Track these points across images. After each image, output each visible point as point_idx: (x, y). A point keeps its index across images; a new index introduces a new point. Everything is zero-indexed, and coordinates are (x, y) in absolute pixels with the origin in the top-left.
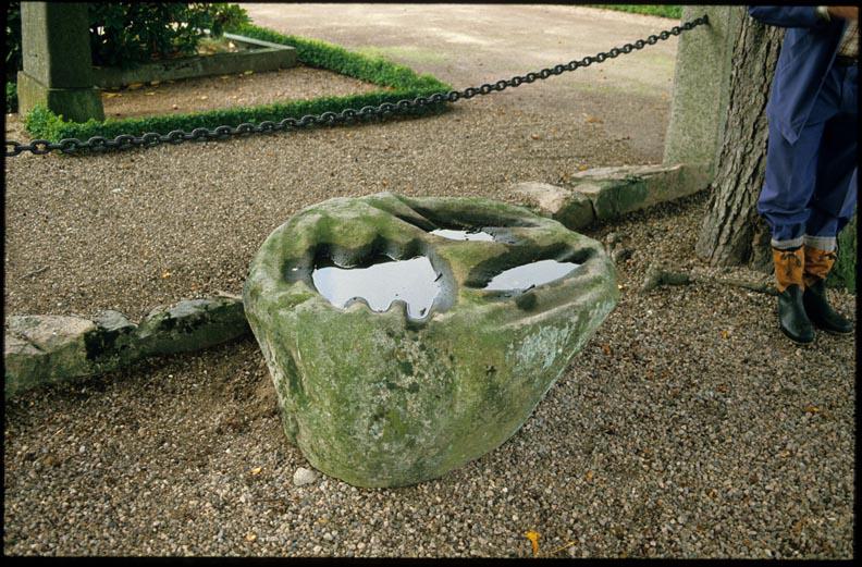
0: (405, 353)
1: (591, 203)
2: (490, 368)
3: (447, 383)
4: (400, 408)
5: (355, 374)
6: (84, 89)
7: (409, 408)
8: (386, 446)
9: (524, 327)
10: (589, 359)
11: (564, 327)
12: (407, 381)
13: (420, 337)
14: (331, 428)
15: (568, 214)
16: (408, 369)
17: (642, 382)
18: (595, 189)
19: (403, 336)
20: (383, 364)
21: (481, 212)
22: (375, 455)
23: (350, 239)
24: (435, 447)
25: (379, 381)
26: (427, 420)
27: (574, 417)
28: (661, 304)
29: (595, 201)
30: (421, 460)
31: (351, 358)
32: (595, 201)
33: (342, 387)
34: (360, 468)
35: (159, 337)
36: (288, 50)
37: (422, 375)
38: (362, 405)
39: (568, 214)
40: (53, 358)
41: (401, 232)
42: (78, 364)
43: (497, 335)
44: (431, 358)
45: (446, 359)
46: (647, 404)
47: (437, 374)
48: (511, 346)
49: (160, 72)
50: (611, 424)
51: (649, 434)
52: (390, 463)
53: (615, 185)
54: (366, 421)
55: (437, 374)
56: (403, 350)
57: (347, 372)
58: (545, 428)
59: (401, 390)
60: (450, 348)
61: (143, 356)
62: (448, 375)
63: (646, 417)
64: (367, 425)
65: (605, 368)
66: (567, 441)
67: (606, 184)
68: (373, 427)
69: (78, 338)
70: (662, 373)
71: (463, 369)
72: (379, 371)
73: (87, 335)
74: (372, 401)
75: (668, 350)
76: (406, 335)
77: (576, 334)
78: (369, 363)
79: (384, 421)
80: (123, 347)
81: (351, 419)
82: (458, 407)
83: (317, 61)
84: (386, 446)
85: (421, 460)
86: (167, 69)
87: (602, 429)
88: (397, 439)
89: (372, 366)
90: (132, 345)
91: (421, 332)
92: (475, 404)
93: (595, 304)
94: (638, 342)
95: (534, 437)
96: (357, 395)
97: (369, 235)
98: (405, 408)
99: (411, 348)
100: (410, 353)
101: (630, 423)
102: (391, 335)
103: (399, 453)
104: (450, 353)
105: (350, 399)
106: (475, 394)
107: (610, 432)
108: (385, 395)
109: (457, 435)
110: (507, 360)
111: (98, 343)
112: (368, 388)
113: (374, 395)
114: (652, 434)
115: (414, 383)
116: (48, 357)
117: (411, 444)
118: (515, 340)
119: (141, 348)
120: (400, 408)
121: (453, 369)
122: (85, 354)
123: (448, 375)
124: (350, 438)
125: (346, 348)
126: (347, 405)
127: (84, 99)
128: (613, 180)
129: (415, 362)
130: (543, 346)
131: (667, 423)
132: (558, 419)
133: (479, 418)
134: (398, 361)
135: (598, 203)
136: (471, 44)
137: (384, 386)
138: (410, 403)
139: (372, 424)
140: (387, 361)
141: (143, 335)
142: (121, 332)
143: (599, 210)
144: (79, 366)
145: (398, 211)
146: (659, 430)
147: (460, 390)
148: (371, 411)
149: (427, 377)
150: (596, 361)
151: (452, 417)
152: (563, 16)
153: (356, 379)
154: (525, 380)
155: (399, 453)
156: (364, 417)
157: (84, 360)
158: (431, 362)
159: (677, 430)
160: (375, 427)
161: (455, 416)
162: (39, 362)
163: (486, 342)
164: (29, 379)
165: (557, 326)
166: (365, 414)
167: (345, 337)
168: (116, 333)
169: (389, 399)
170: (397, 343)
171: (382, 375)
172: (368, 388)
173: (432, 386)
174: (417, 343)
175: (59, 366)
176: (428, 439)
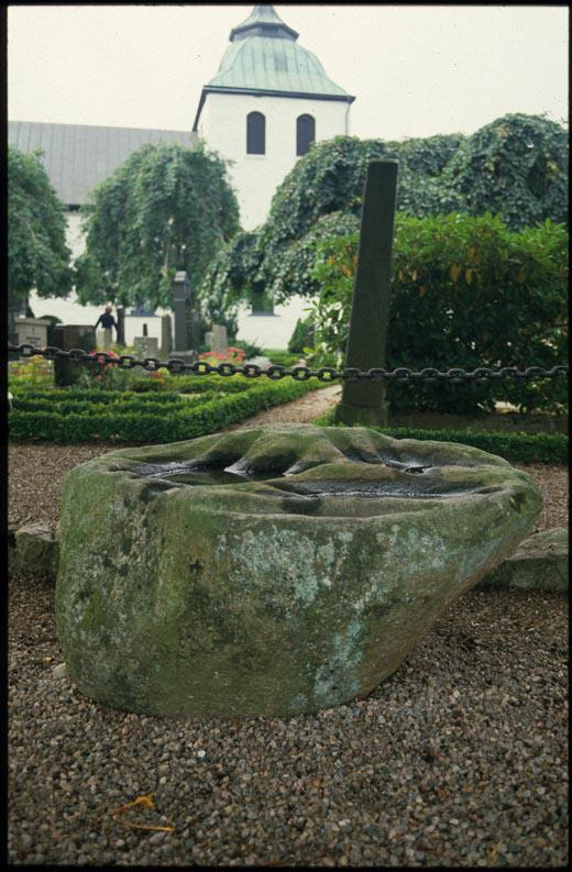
11: (326, 543)
12: (122, 559)
25: (99, 554)
38: (75, 577)
45: (159, 541)
48: (224, 539)
85: (121, 672)
89: (98, 535)
92: (177, 609)
98: (109, 592)
113: (88, 568)
115: (126, 565)
117: (106, 640)
120: (104, 591)
130: (283, 558)
137: (101, 561)
138: (115, 587)
139: (76, 602)
140: (114, 533)
143: (514, 402)
147: (161, 583)
149: (139, 560)
151: (150, 620)
153: (81, 546)
156: (73, 592)
158: (147, 542)
160: (78, 607)
161: (155, 620)
164: (34, 562)
165: (310, 535)
166: (73, 588)
171: (104, 548)
176: (124, 644)
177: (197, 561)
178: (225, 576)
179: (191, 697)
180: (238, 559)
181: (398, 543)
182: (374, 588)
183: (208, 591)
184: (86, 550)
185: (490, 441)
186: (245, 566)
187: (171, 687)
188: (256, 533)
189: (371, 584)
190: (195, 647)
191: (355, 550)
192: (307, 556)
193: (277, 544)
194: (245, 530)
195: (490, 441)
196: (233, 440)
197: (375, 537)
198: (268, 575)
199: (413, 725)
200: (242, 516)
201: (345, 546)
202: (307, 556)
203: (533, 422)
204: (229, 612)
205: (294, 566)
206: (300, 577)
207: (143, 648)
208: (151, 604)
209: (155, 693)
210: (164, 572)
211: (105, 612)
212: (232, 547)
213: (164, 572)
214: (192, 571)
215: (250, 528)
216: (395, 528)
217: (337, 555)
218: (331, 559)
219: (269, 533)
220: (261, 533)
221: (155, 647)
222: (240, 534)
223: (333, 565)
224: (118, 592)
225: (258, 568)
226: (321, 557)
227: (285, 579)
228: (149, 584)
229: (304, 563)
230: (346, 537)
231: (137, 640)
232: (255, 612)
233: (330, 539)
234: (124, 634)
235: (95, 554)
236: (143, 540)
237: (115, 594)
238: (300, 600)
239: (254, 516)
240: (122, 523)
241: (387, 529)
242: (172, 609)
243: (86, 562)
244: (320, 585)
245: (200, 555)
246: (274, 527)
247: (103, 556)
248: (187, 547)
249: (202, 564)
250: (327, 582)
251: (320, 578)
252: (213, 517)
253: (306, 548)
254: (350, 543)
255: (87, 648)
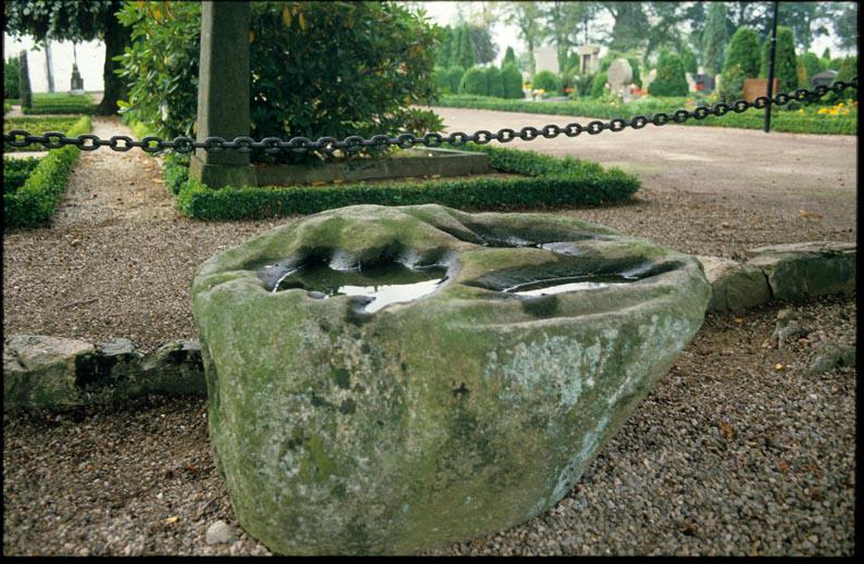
0: (343, 355)
1: (767, 277)
2: (458, 386)
3: (396, 403)
4: (326, 435)
5: (270, 380)
6: (238, 166)
7: (338, 435)
8: (302, 490)
9: (517, 331)
10: (694, 439)
11: (592, 343)
12: (340, 395)
13: (364, 334)
14: (236, 455)
15: (729, 287)
16: (343, 379)
17: (765, 473)
18: (771, 261)
19: (342, 332)
20: (309, 369)
21: (549, 228)
22: (288, 502)
23: (356, 241)
24: (377, 501)
25: (301, 392)
26: (362, 455)
27: (637, 506)
28: (834, 389)
29: (771, 275)
30: (358, 522)
31: (267, 357)
32: (771, 275)
33: (250, 395)
34: (271, 520)
35: (166, 371)
36: (480, 156)
37: (360, 389)
38: (273, 423)
39: (729, 287)
40: (33, 379)
41: (426, 238)
42: (64, 389)
43: (469, 335)
44: (375, 364)
45: (396, 368)
46: (762, 501)
47: (383, 389)
48: (494, 356)
49: (345, 172)
50: (694, 521)
51: (752, 542)
52: (311, 519)
53: (801, 257)
54: (277, 448)
55: (383, 389)
56: (340, 352)
57: (260, 375)
58: (587, 513)
59: (331, 408)
60: (402, 352)
61: (146, 392)
62: (398, 392)
63: (755, 518)
64: (277, 454)
65: (714, 451)
66: (613, 535)
67: (788, 255)
68: (286, 458)
69: (68, 360)
70: (804, 466)
71: (419, 383)
72: (304, 377)
73: (79, 358)
74: (287, 420)
75: (823, 440)
76: (345, 329)
77: (618, 362)
78: (290, 366)
79: (302, 451)
80: (121, 378)
81: (256, 443)
82: (410, 443)
83: (507, 165)
84: (302, 490)
85: (358, 522)
86: (352, 169)
87: (678, 526)
88: (318, 480)
90: (132, 377)
91: (365, 326)
92: (437, 441)
93: (649, 318)
94: (780, 427)
95: (563, 524)
96: (268, 408)
97: (382, 238)
98: (333, 435)
99: (351, 349)
100: (350, 357)
101: (725, 523)
102: (325, 328)
103: (322, 503)
104: (403, 358)
105: (258, 413)
106: (436, 424)
107: (689, 532)
108: (306, 413)
109: (412, 488)
110: (487, 377)
111: (92, 369)
112: (284, 400)
113: (291, 411)
114: (758, 543)
115: (350, 400)
116: (27, 376)
117: (339, 491)
118: (500, 347)
119: (143, 382)
120: (326, 435)
121: (405, 383)
122: (74, 379)
123: (398, 392)
124: (256, 471)
125: (262, 341)
126: (253, 423)
127: (237, 176)
128: (799, 253)
129: (354, 369)
130: (552, 367)
131: (786, 530)
132: (611, 504)
133: (448, 466)
134: (331, 366)
135: (775, 277)
136: (691, 161)
137: (308, 400)
138: (341, 429)
139: (285, 453)
140: (316, 365)
141: (147, 367)
142: (119, 358)
144: (65, 393)
145: (439, 222)
146: (770, 538)
147: (413, 415)
148: (284, 434)
149: (368, 392)
150: (704, 443)
151: (402, 458)
152: (812, 142)
154: (525, 418)
155: (322, 503)
156: (275, 442)
157: (71, 386)
158: (376, 371)
159: (800, 541)
160: (289, 458)
161: (407, 457)
162: (16, 379)
163: (454, 345)
165: (578, 338)
166: (275, 437)
167: (263, 327)
168: (113, 359)
169: (312, 420)
170: (333, 341)
171: (306, 384)
172: (284, 400)
173: (375, 406)
174: (359, 343)
175: (41, 388)
176: (365, 489)
177: (463, 385)
178: (494, 396)
179: (435, 529)
180: (509, 376)
181: (657, 332)
182: (628, 380)
183: (476, 414)
184: (280, 389)
185: (384, 193)
186: (516, 380)
187: (415, 525)
188: (528, 344)
189: (626, 377)
190: (453, 476)
191: (619, 346)
192: (575, 360)
193: (548, 352)
194: (517, 343)
195: (384, 193)
196: (316, 231)
197: (637, 328)
198: (538, 386)
199: (646, 504)
200: (506, 328)
201: (611, 343)
202: (575, 360)
203: (368, 168)
204: (495, 432)
205: (563, 372)
206: (568, 382)
207: (391, 490)
208: (400, 441)
209: (395, 535)
210: (415, 402)
211: (332, 459)
212: (504, 364)
213: (415, 402)
214: (455, 395)
215: (523, 340)
216: (655, 318)
217: (603, 354)
218: (597, 359)
219: (540, 342)
220: (533, 344)
221: (406, 487)
222: (512, 348)
223: (597, 365)
224: (347, 433)
225: (528, 380)
226: (588, 358)
227: (553, 387)
228: (396, 418)
229: (572, 368)
230: (612, 334)
231: (385, 483)
232: (520, 427)
233: (597, 339)
234: (366, 479)
235: (296, 394)
236: (367, 368)
237: (343, 437)
238: (565, 406)
239: (520, 325)
240: (325, 352)
241: (648, 321)
242: (431, 442)
243: (285, 404)
244: (583, 387)
245: (465, 377)
246: (545, 335)
247: (308, 394)
248: (447, 371)
249: (468, 387)
250: (591, 382)
251: (584, 380)
252: (479, 334)
253: (574, 351)
254: (615, 340)
255: (311, 504)
